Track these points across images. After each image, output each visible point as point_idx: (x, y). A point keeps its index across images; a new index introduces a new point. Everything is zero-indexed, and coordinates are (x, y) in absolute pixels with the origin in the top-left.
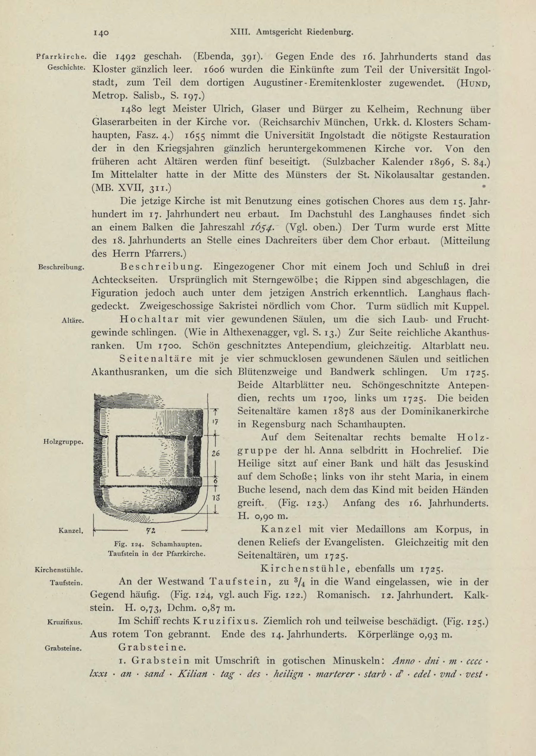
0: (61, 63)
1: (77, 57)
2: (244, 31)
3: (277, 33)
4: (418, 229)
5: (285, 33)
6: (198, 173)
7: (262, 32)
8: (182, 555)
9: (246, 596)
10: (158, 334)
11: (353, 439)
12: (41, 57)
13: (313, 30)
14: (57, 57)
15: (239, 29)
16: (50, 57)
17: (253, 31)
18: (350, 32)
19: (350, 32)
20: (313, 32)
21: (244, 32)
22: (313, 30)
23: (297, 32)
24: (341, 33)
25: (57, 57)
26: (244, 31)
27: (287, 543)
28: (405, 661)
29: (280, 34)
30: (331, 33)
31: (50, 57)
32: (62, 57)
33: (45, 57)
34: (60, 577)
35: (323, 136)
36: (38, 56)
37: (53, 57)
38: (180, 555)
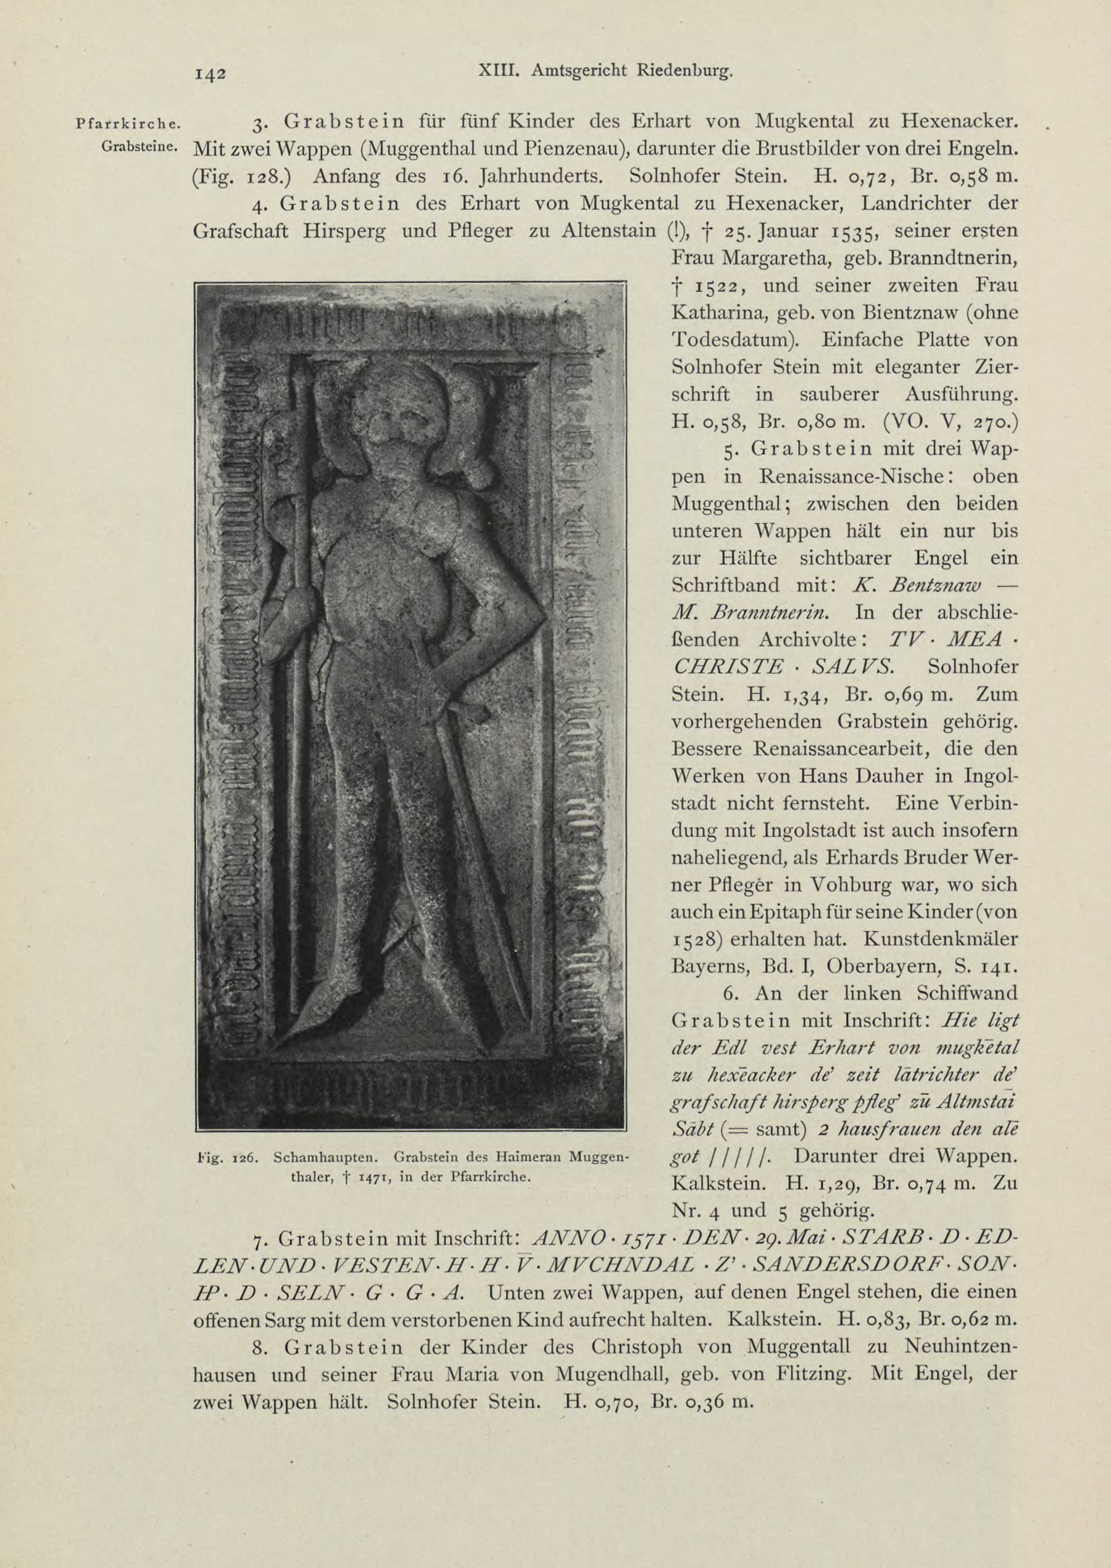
0: (130, 139)
1: (161, 124)
2: (507, 68)
3: (575, 74)
4: (985, 397)
5: (590, 72)
6: (941, 772)
7: (544, 72)
8: (484, 1178)
9: (687, 915)
10: (823, 1294)
11: (788, 914)
12: (87, 124)
13: (650, 66)
14: (120, 126)
15: (496, 65)
16: (104, 125)
17: (525, 67)
18: (726, 69)
19: (726, 69)
20: (649, 71)
21: (507, 71)
22: (650, 66)
23: (619, 71)
24: (708, 72)
25: (120, 126)
26: (506, 69)
27: (962, 752)
28: (759, 614)
29: (581, 74)
30: (686, 72)
31: (104, 125)
32: (131, 125)
33: (94, 125)
34: (306, 1169)
35: (851, 1023)
36: (80, 122)
37: (112, 125)
38: (478, 1178)
